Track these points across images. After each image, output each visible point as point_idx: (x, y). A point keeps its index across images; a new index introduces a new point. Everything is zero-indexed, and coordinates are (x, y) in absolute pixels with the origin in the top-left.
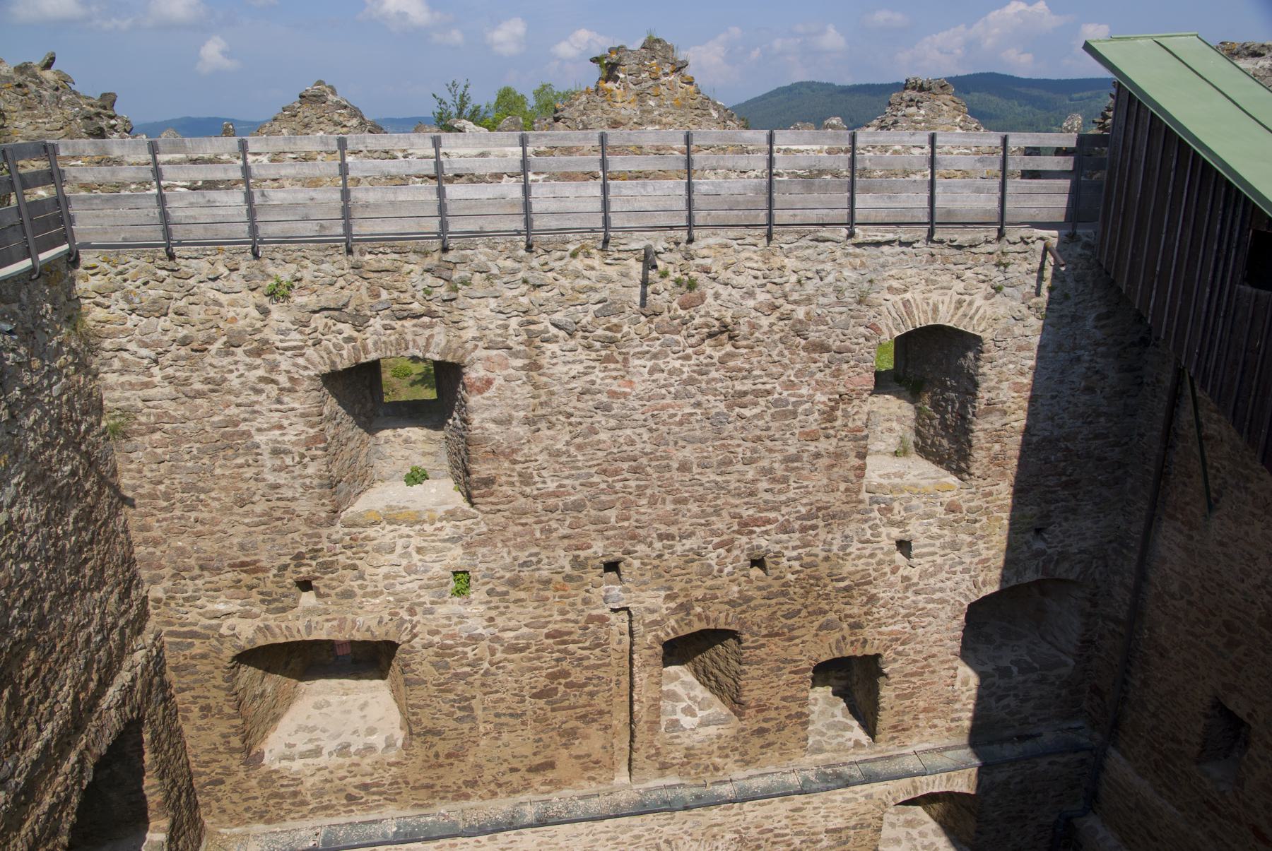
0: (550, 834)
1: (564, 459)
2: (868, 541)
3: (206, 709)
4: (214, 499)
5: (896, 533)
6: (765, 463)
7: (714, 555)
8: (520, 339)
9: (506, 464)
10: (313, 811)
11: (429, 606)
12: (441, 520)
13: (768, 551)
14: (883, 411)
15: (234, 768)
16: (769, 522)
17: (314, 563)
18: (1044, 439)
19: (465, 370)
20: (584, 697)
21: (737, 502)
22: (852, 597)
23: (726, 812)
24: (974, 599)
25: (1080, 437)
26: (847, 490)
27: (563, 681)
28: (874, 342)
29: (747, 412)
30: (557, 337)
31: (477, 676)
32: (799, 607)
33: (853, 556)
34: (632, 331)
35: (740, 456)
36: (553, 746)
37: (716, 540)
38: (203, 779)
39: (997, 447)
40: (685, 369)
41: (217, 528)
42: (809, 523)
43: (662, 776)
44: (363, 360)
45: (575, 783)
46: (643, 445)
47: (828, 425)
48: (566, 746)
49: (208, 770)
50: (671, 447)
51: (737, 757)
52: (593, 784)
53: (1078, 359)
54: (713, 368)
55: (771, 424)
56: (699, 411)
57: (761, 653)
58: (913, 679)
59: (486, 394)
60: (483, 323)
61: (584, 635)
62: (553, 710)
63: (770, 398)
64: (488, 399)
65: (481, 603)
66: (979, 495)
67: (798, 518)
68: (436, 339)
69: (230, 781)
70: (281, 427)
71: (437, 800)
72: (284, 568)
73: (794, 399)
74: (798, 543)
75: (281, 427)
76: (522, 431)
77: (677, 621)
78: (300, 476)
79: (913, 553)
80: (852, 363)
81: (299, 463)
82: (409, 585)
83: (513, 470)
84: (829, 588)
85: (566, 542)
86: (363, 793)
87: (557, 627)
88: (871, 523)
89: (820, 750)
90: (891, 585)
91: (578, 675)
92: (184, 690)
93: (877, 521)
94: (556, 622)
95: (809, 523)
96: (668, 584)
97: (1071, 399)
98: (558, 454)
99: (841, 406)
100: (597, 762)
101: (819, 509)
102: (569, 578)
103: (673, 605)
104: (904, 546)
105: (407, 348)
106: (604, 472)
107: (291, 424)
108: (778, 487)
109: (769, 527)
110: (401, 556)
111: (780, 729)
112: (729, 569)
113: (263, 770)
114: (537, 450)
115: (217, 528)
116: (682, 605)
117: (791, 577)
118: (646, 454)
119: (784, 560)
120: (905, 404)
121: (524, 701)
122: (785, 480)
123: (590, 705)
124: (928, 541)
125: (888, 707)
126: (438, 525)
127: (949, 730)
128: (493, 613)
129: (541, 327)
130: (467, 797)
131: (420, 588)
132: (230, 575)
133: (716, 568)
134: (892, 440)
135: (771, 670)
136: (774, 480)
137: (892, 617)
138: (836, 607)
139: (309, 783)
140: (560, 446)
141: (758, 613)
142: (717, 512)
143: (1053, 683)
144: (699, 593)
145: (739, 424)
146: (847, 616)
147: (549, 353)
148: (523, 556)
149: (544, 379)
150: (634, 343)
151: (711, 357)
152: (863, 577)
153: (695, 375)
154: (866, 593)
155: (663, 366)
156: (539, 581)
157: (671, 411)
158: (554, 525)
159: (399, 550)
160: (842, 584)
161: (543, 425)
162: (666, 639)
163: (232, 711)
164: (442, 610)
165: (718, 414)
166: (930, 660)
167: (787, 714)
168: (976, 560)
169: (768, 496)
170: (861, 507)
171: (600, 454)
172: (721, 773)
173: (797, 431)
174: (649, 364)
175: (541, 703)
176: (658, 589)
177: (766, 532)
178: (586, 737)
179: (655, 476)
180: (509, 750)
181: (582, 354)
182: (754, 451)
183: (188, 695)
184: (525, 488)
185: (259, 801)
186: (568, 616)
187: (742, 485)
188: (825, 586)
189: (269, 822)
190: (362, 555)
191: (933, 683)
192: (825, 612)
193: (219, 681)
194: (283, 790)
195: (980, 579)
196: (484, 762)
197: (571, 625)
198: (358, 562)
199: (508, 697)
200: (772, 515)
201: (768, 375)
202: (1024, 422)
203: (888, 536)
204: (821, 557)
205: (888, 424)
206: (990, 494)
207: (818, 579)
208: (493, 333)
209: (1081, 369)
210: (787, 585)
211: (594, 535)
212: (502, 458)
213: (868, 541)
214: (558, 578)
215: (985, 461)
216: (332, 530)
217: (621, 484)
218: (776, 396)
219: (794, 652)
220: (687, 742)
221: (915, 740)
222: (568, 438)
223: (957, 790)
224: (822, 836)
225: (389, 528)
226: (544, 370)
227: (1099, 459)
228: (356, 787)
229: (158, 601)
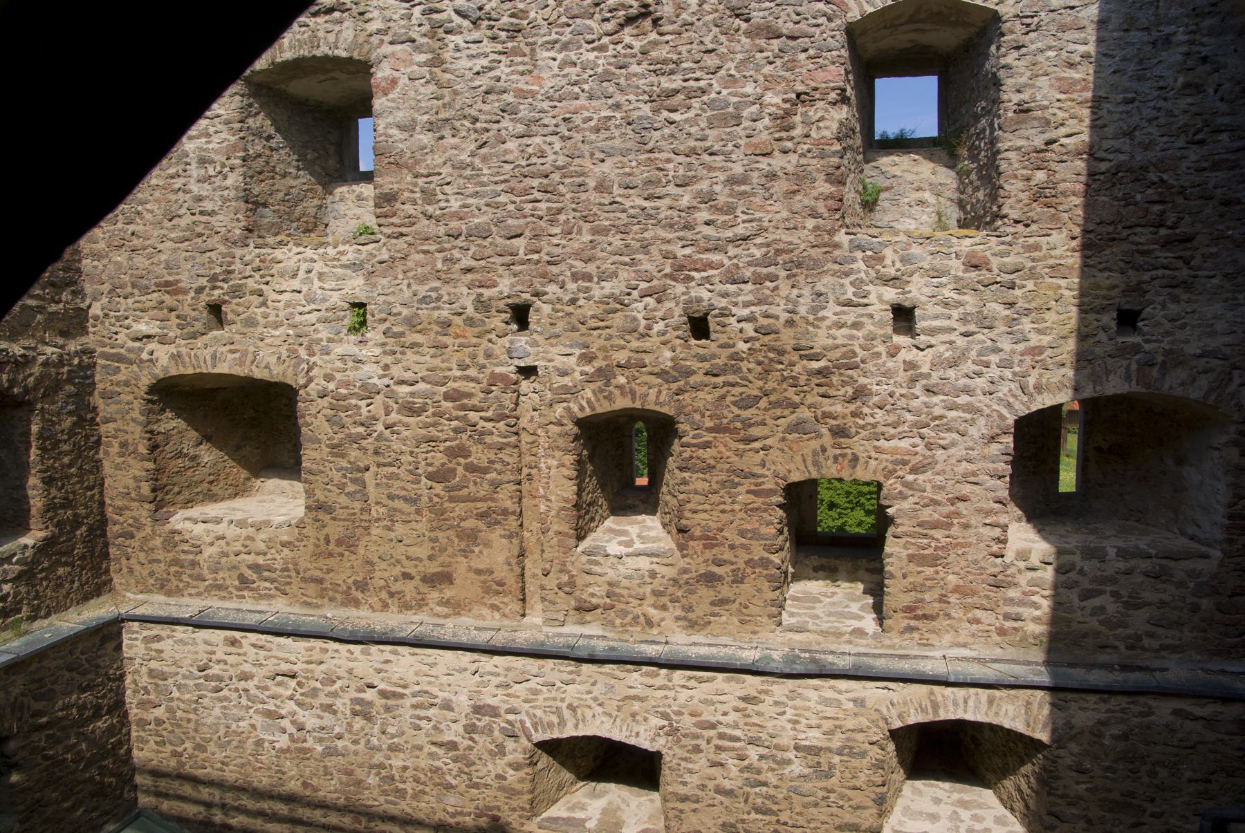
0: (430, 660)
1: (468, 172)
2: (849, 304)
3: (124, 445)
4: (148, 210)
5: (891, 294)
6: (704, 186)
7: (640, 306)
8: (424, 29)
9: (409, 178)
10: (208, 589)
11: (325, 343)
12: (345, 242)
13: (712, 307)
14: (910, 177)
15: (143, 520)
16: (711, 265)
17: (226, 286)
18: (1119, 166)
19: (373, 70)
20: (486, 486)
21: (670, 236)
22: (830, 385)
23: (650, 681)
24: (1023, 411)
25: (1184, 165)
26: (816, 228)
27: (462, 460)
28: (839, 22)
29: (676, 117)
30: (460, 27)
31: (370, 440)
32: (756, 392)
33: (828, 322)
34: (539, 17)
35: (671, 173)
36: (450, 550)
37: (643, 285)
38: (116, 528)
39: (1041, 176)
40: (600, 62)
41: (148, 242)
42: (765, 271)
43: (583, 623)
44: (279, 60)
45: (475, 610)
46: (553, 157)
47: (784, 134)
48: (465, 553)
49: (121, 519)
50: (587, 163)
51: (679, 612)
52: (497, 615)
53: (1167, 40)
54: (633, 60)
55: (707, 132)
56: (618, 115)
57: (707, 454)
58: (934, 533)
59: (391, 96)
60: (388, 13)
61: (485, 400)
62: (451, 499)
63: (705, 98)
64: (393, 100)
65: (376, 345)
66: (1018, 248)
67: (750, 264)
68: (344, 34)
69: (139, 535)
70: (208, 135)
71: (326, 600)
72: (200, 290)
73: (735, 99)
74: (750, 298)
75: (208, 135)
76: (426, 138)
77: (594, 392)
78: (220, 187)
79: (920, 325)
80: (812, 52)
81: (220, 172)
82: (307, 316)
83: (415, 185)
84: (798, 368)
85: (470, 276)
86: (255, 577)
87: (455, 385)
88: (852, 278)
89: (800, 630)
90: (888, 374)
91: (479, 455)
92: (108, 422)
93: (863, 275)
94: (455, 379)
95: (765, 271)
96: (582, 340)
97: (1161, 104)
98: (462, 166)
99: (801, 109)
100: (501, 584)
101: (778, 252)
102: (470, 322)
103: (589, 369)
104: (903, 316)
105: (318, 46)
106: (511, 191)
107: (216, 132)
108: (722, 218)
109: (711, 272)
110: (303, 282)
111: (738, 580)
112: (659, 326)
113: (168, 527)
114: (440, 161)
115: (148, 242)
116: (599, 370)
117: (743, 346)
118: (558, 168)
119: (732, 320)
120: (942, 171)
121: (419, 482)
122: (730, 209)
123: (493, 500)
124: (939, 310)
125: (899, 574)
126: (341, 248)
127: (1002, 632)
128: (388, 360)
129: (443, 16)
130: (357, 603)
131: (319, 321)
132: (155, 295)
133: (643, 323)
134: (925, 217)
135: (723, 484)
136: (719, 210)
137: (895, 425)
138: (810, 399)
139: (208, 551)
140: (464, 157)
141: (701, 395)
142: (645, 248)
143: (1181, 584)
144: (622, 357)
145: (667, 131)
146: (827, 415)
147: (452, 46)
148: (422, 290)
149: (448, 76)
150: (542, 32)
151: (631, 47)
152: (844, 356)
153: (612, 69)
154: (852, 380)
155: (574, 58)
156: (438, 323)
157: (586, 114)
158: (456, 254)
159: (302, 274)
160: (815, 365)
161: (447, 132)
162: (580, 415)
163: (146, 451)
164: (339, 350)
165: (640, 118)
166: (960, 505)
167: (747, 557)
168: (1020, 347)
169: (709, 231)
170: (837, 253)
171: (508, 167)
172: (655, 631)
173: (742, 142)
174: (560, 57)
175: (439, 488)
176: (571, 346)
177: (707, 280)
178: (487, 545)
179: (568, 196)
180: (401, 549)
181: (487, 46)
182: (689, 167)
183: (111, 426)
184: (427, 207)
185: (162, 565)
186: (468, 372)
187: (675, 213)
188: (792, 364)
189: (169, 594)
190: (268, 278)
191: (968, 545)
192: (795, 406)
193: (136, 414)
194: (183, 557)
195: (1031, 381)
196: (376, 560)
197: (472, 384)
198: (264, 287)
199: (402, 472)
200: (715, 257)
201: (701, 69)
202: (1085, 137)
203: (880, 298)
204: (782, 320)
205: (919, 195)
206: (1037, 247)
207: (781, 352)
208: (398, 28)
209: (1173, 56)
210: (736, 357)
211: (501, 270)
212: (405, 171)
213: (849, 304)
214: (458, 320)
215: (1024, 196)
216: (245, 250)
217: (530, 206)
218: (713, 95)
219: (751, 461)
220: (611, 574)
221: (947, 638)
222: (473, 147)
223: (1007, 724)
224: (791, 755)
225: (296, 250)
226: (448, 65)
227: (1227, 203)
228: (249, 567)
229: (96, 318)
